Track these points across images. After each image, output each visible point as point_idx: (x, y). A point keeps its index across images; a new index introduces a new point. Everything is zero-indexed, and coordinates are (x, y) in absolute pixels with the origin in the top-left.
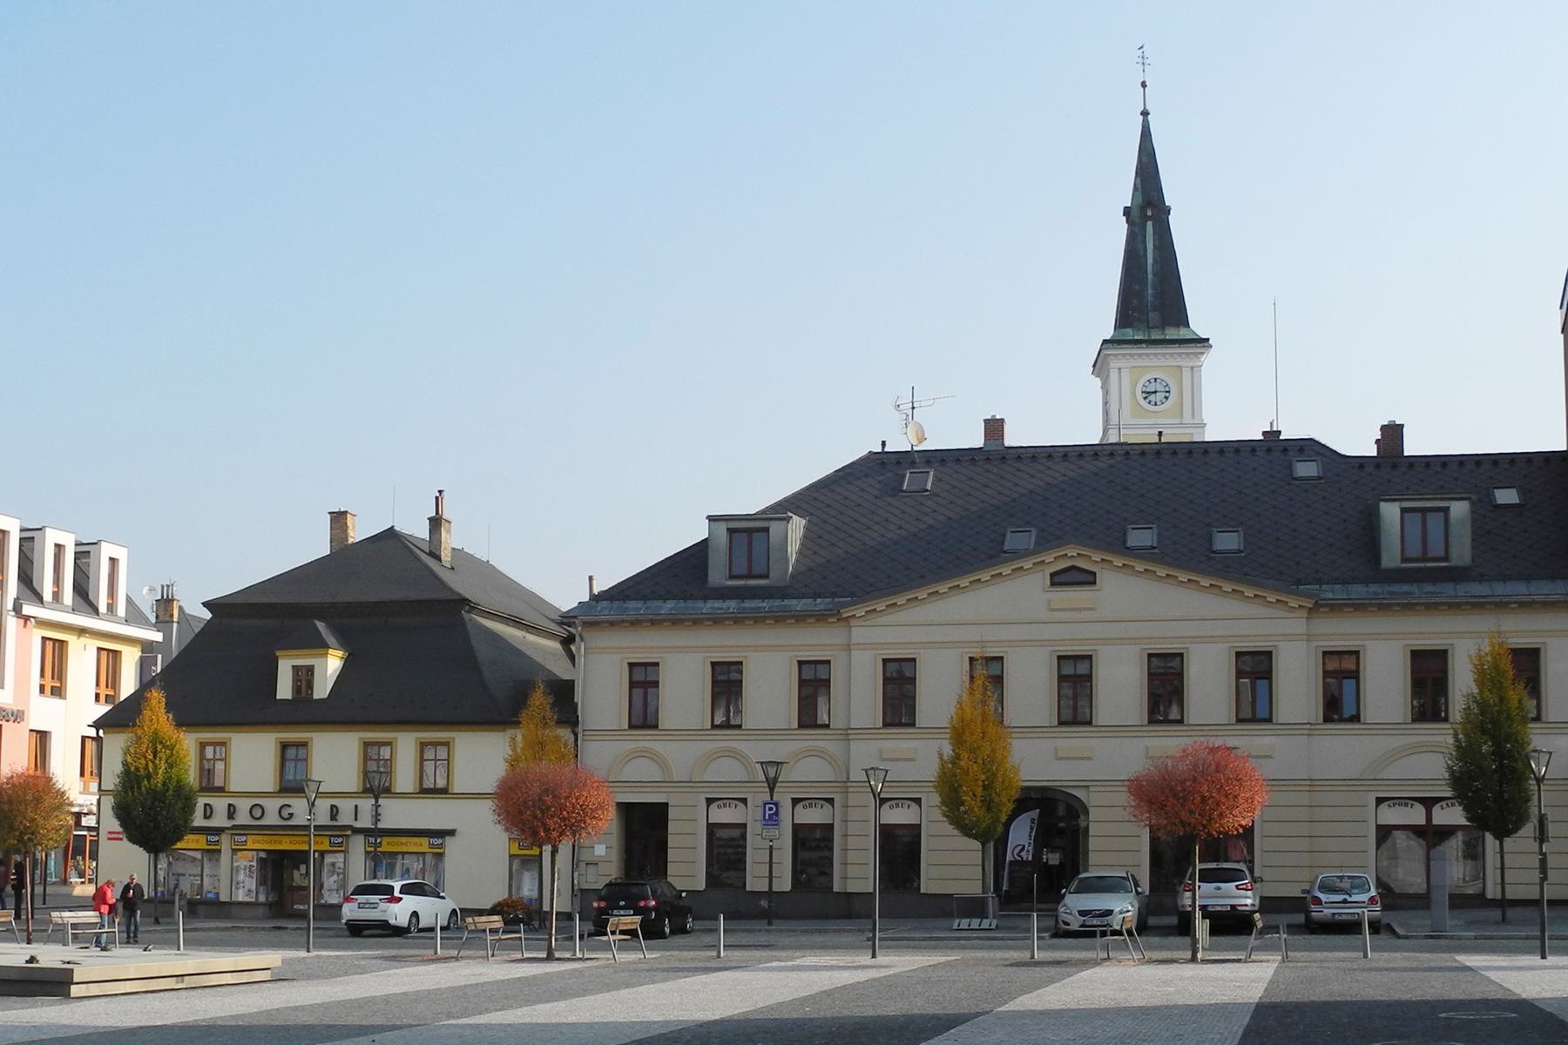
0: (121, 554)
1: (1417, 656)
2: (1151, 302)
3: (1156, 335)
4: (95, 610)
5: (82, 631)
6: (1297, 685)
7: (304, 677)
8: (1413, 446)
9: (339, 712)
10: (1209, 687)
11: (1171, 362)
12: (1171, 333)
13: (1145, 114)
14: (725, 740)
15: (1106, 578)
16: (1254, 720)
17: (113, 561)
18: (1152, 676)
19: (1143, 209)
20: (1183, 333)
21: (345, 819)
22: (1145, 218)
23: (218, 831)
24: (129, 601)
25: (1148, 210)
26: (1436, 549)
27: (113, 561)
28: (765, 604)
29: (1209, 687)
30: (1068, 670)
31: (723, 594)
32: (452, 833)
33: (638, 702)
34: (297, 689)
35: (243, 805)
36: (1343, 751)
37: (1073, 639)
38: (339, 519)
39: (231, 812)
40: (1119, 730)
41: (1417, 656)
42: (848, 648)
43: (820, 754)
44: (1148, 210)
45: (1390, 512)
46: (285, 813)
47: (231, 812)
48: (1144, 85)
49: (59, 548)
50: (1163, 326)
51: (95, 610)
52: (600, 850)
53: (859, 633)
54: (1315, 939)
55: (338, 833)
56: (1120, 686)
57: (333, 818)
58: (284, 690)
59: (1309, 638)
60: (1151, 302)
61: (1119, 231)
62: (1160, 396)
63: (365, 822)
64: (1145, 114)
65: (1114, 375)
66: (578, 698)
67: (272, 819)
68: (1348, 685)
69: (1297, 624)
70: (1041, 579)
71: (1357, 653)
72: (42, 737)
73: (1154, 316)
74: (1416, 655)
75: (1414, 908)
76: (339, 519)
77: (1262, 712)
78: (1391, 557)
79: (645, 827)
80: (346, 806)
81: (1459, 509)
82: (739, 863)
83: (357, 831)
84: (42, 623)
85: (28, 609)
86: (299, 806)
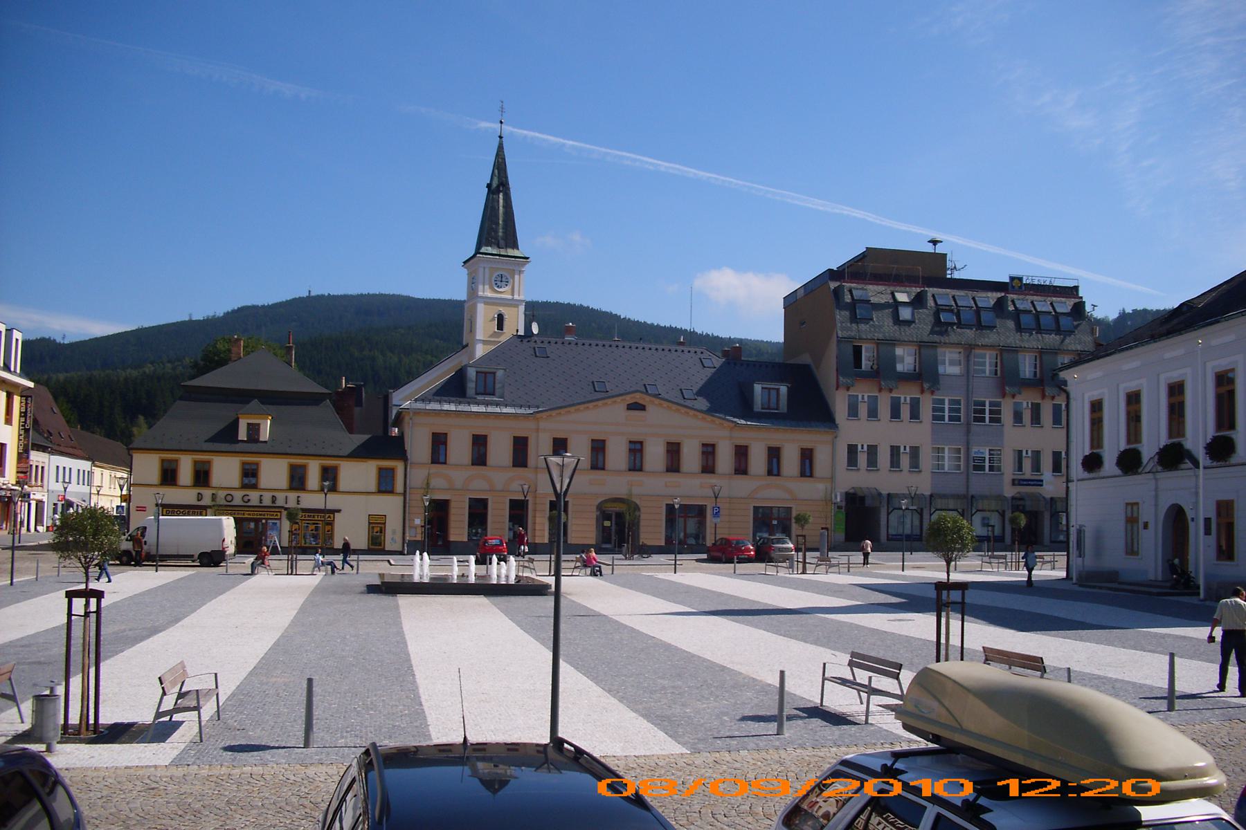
2: (498, 229)
6: (655, 455)
7: (254, 430)
10: (691, 457)
12: (511, 252)
15: (649, 408)
16: (634, 470)
18: (668, 451)
19: (498, 187)
24: (423, 399)
26: (773, 404)
28: (498, 410)
29: (691, 457)
32: (339, 511)
33: (600, 458)
34: (249, 435)
35: (221, 494)
36: (742, 486)
39: (214, 497)
40: (618, 472)
42: (537, 430)
44: (500, 166)
45: (758, 388)
46: (246, 499)
50: (507, 247)
53: (542, 425)
56: (655, 455)
57: (273, 502)
58: (242, 434)
60: (498, 229)
63: (292, 504)
67: (237, 501)
68: (442, 447)
70: (623, 406)
71: (641, 443)
73: (502, 242)
77: (600, 465)
78: (758, 407)
79: (438, 513)
80: (281, 498)
81: (784, 389)
82: (382, 531)
86: (207, 493)
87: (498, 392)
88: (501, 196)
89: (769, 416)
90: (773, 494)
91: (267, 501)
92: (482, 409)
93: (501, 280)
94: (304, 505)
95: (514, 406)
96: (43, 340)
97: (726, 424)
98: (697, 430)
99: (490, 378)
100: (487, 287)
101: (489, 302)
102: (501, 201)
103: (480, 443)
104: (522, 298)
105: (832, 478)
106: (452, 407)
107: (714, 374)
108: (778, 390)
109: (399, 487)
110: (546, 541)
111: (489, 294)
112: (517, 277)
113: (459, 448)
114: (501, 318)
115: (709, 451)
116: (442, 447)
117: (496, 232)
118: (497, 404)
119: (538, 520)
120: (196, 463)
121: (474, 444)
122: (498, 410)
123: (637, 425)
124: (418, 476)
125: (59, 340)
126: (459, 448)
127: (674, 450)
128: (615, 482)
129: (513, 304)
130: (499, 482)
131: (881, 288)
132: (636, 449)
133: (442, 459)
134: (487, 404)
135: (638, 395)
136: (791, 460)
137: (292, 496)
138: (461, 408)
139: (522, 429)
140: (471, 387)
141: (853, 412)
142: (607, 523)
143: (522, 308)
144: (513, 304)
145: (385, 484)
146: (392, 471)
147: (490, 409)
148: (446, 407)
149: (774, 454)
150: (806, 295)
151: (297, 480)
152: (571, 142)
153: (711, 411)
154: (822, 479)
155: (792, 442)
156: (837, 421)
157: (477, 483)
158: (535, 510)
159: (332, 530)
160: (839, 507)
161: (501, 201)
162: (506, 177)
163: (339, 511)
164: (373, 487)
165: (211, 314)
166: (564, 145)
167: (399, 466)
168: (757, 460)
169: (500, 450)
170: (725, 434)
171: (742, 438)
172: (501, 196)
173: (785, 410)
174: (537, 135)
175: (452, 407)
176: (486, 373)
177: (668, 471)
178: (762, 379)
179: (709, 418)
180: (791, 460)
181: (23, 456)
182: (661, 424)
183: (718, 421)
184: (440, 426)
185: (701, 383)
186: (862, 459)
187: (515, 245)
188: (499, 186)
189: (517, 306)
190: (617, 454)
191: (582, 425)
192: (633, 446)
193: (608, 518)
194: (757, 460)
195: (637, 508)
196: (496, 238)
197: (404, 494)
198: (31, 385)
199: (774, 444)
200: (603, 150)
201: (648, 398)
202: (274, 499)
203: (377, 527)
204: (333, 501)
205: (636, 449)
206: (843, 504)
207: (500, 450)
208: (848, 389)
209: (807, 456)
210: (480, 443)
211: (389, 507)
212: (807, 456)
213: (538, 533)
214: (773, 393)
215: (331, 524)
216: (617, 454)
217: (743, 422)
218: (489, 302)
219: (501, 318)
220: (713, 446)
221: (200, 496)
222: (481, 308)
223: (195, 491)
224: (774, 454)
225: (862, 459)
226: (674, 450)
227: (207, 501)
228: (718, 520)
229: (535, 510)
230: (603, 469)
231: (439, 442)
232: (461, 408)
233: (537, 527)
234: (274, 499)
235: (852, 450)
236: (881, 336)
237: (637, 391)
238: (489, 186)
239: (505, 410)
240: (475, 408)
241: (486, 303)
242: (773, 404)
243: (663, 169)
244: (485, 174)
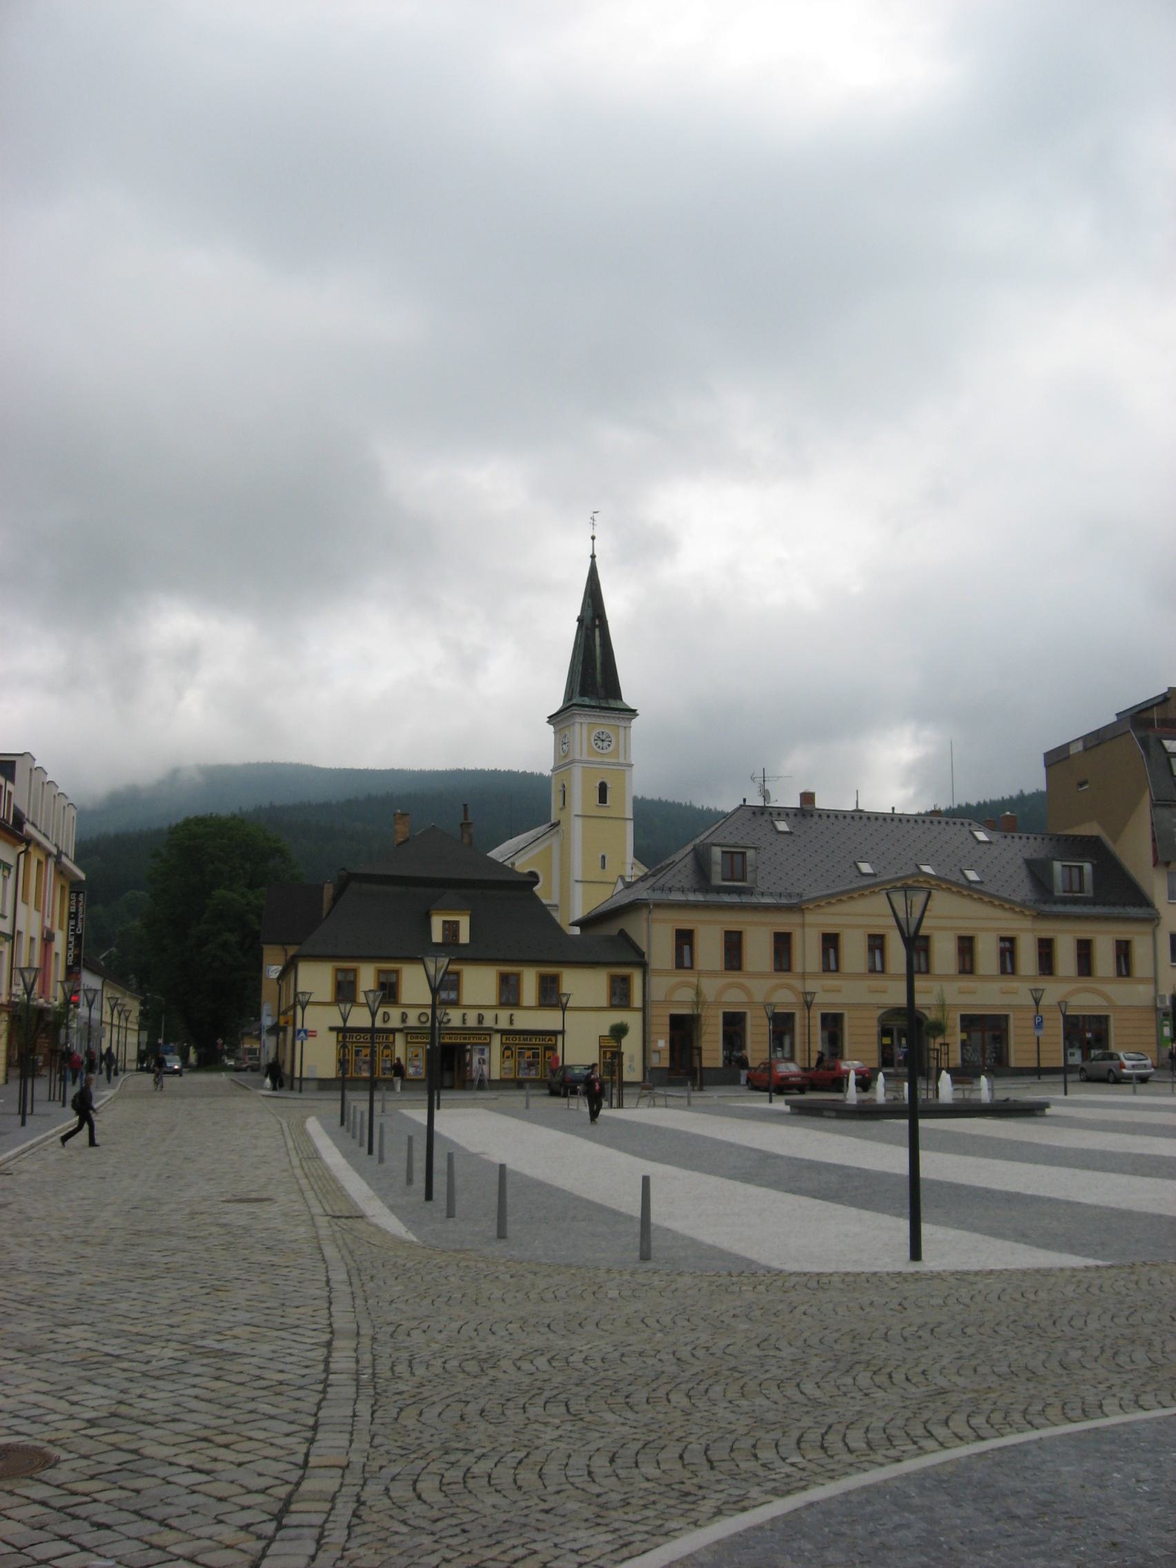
1: (728, 934)
8: (821, 803)
9: (475, 955)
10: (987, 954)
11: (612, 722)
12: (613, 704)
13: (593, 557)
14: (784, 979)
20: (613, 704)
21: (489, 1022)
22: (595, 626)
23: (393, 1031)
29: (987, 954)
31: (720, 890)
39: (404, 1017)
41: (728, 934)
42: (803, 925)
43: (789, 987)
45: (1057, 866)
47: (404, 1017)
48: (593, 538)
53: (810, 918)
54: (1089, 1085)
55: (483, 1033)
57: (464, 1021)
58: (437, 936)
62: (606, 744)
63: (503, 1024)
64: (593, 557)
69: (1027, 924)
74: (870, 936)
77: (968, 968)
79: (683, 1029)
81: (1087, 867)
83: (497, 1031)
86: (395, 1013)
87: (750, 876)
91: (472, 1022)
94: (518, 1025)
96: (187, 822)
99: (737, 858)
105: (1155, 980)
108: (1081, 868)
109: (637, 1001)
110: (720, 1064)
115: (1008, 948)
121: (1040, 946)
124: (661, 986)
128: (987, 993)
137: (504, 1015)
145: (620, 995)
149: (1085, 950)
150: (1086, 749)
151: (509, 994)
154: (1142, 980)
160: (1166, 1015)
197: (644, 1009)
198: (82, 876)
199: (1044, 935)
202: (481, 1019)
206: (1170, 1010)
209: (1123, 951)
212: (1123, 951)
214: (1075, 872)
215: (553, 1048)
220: (740, 933)
224: (1085, 950)
226: (966, 946)
228: (1040, 1033)
234: (481, 1019)
242: (1076, 887)
244: (574, 606)
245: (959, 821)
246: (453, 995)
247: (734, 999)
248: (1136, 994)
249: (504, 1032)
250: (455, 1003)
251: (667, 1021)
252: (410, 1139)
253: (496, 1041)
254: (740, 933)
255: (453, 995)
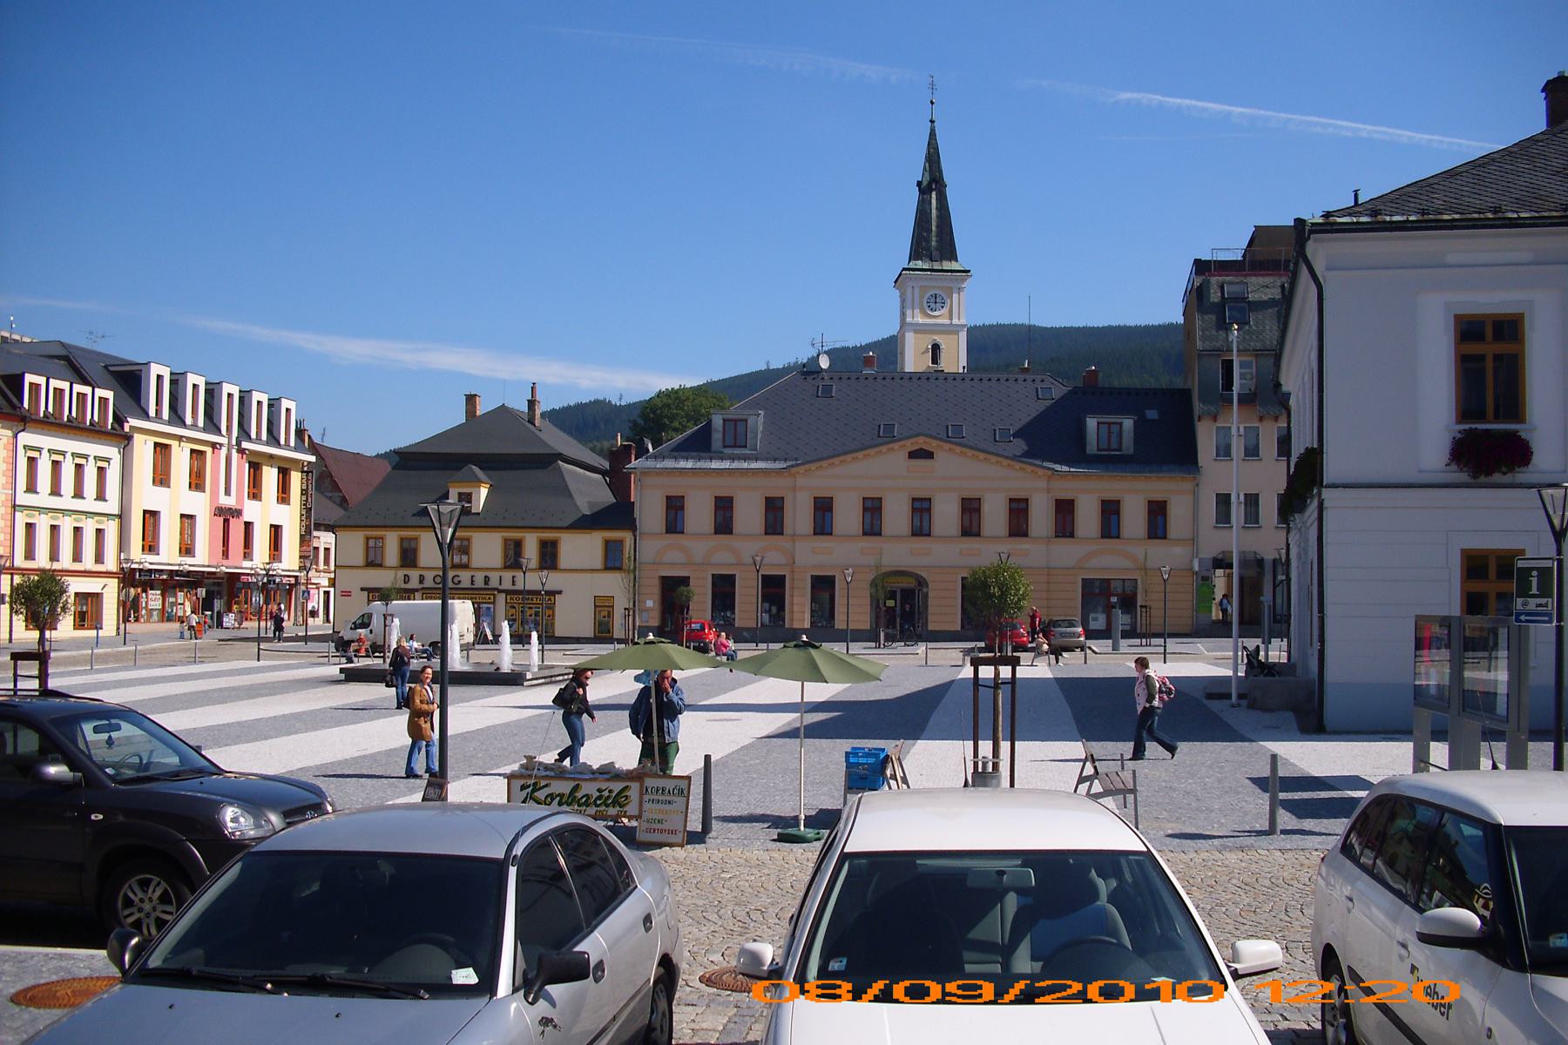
0: (292, 405)
2: (933, 239)
3: (936, 266)
4: (218, 431)
5: (180, 438)
6: (946, 514)
7: (466, 498)
9: (485, 523)
10: (995, 516)
12: (947, 265)
17: (288, 410)
19: (930, 184)
20: (954, 266)
21: (494, 583)
25: (933, 183)
27: (288, 410)
28: (745, 465)
29: (995, 516)
30: (917, 505)
32: (560, 592)
35: (429, 575)
36: (1066, 553)
37: (921, 488)
38: (471, 399)
39: (422, 579)
42: (794, 489)
45: (1091, 423)
49: (159, 377)
51: (183, 424)
52: (650, 603)
53: (800, 481)
56: (946, 514)
57: (486, 583)
59: (1049, 490)
60: (933, 239)
61: (910, 199)
63: (507, 585)
65: (909, 290)
66: (637, 515)
68: (975, 516)
72: (248, 525)
74: (1011, 500)
75: (241, 699)
76: (471, 399)
77: (975, 530)
78: (1092, 447)
79: (673, 592)
80: (494, 577)
81: (1128, 423)
82: (610, 615)
83: (500, 591)
84: (190, 440)
85: (245, 445)
86: (414, 574)
88: (934, 195)
89: (1110, 460)
90: (1110, 562)
91: (479, 583)
92: (726, 464)
93: (936, 301)
95: (767, 459)
96: (597, 402)
97: (1040, 472)
98: (998, 480)
99: (740, 427)
100: (917, 311)
101: (920, 329)
102: (934, 202)
103: (724, 506)
104: (963, 321)
105: (1194, 540)
106: (690, 464)
107: (1048, 410)
111: (920, 319)
112: (955, 296)
113: (699, 514)
114: (936, 348)
116: (1114, 518)
117: (928, 241)
118: (745, 458)
119: (796, 600)
120: (402, 540)
122: (745, 465)
123: (921, 479)
125: (615, 401)
126: (699, 514)
127: (971, 509)
128: (898, 551)
129: (952, 330)
130: (748, 553)
131: (1268, 280)
132: (921, 508)
133: (1114, 532)
134: (733, 458)
135: (921, 440)
136: (1134, 518)
137: (507, 575)
138: (700, 465)
139: (776, 487)
140: (717, 437)
141: (1224, 451)
142: (891, 603)
143: (963, 336)
144: (952, 330)
145: (612, 560)
146: (621, 542)
147: (736, 465)
148: (682, 464)
149: (1110, 511)
151: (513, 558)
152: (1240, 110)
153: (1029, 454)
154: (1179, 541)
155: (1134, 493)
156: (1201, 462)
157: (774, 556)
158: (792, 588)
159: (553, 616)
161: (934, 202)
162: (940, 171)
163: (560, 592)
164: (598, 562)
165: (792, 361)
166: (1229, 114)
167: (627, 536)
168: (1088, 517)
169: (749, 515)
170: (1040, 486)
171: (1065, 490)
172: (934, 195)
173: (1131, 451)
174: (1194, 102)
175: (690, 464)
176: (735, 421)
177: (914, 534)
178: (1094, 412)
179: (1017, 465)
180: (1134, 518)
181: (305, 539)
182: (954, 474)
183: (1029, 468)
184: (675, 487)
185: (1025, 420)
186: (1237, 512)
187: (953, 256)
188: (933, 183)
189: (957, 333)
190: (897, 516)
191: (848, 481)
192: (1015, 505)
193: (892, 595)
194: (1088, 517)
195: (921, 582)
196: (928, 248)
200: (1283, 115)
201: (934, 443)
203: (603, 607)
204: (553, 580)
205: (921, 508)
207: (749, 515)
208: (1215, 419)
209: (1157, 513)
210: (724, 506)
211: (614, 585)
212: (1157, 513)
213: (796, 616)
215: (552, 607)
216: (897, 516)
217: (1065, 468)
218: (920, 329)
219: (936, 348)
220: (730, 500)
221: (407, 579)
222: (910, 337)
223: (401, 573)
224: (1110, 511)
225: (1237, 512)
226: (971, 509)
227: (414, 584)
229: (792, 588)
230: (1118, 537)
231: (675, 506)
232: (700, 465)
233: (796, 608)
235: (1224, 501)
236: (1259, 345)
237: (918, 435)
238: (919, 184)
239: (754, 465)
240: (715, 465)
241: (916, 332)
242: (1114, 446)
243: (1364, 134)
245: (994, 376)
246: (465, 559)
247: (774, 563)
248: (1167, 557)
249: (507, 592)
250: (466, 567)
251: (657, 582)
252: (1012, 785)
253: (501, 598)
254: (730, 500)
255: (465, 559)
